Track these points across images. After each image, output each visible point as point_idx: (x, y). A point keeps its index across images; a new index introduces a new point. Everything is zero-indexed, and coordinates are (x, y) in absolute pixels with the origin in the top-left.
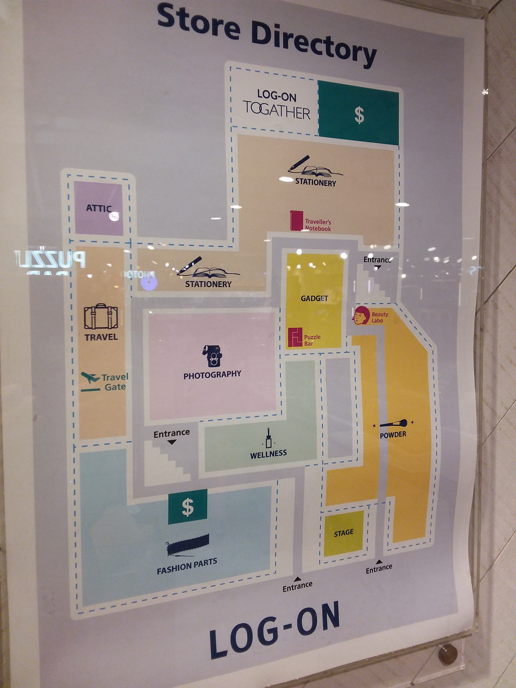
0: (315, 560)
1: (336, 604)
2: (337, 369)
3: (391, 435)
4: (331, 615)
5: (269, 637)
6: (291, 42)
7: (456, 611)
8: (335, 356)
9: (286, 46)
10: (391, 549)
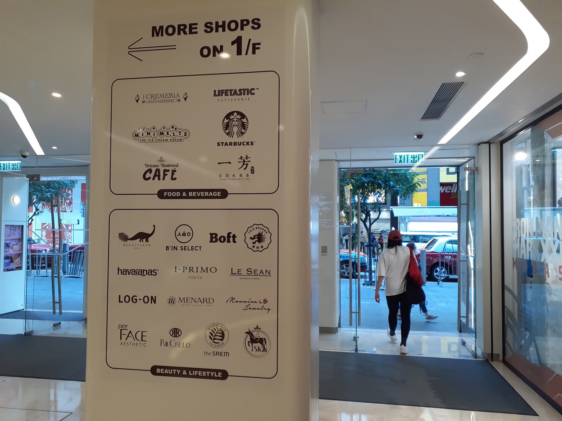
1: (227, 354)
5: (135, 301)
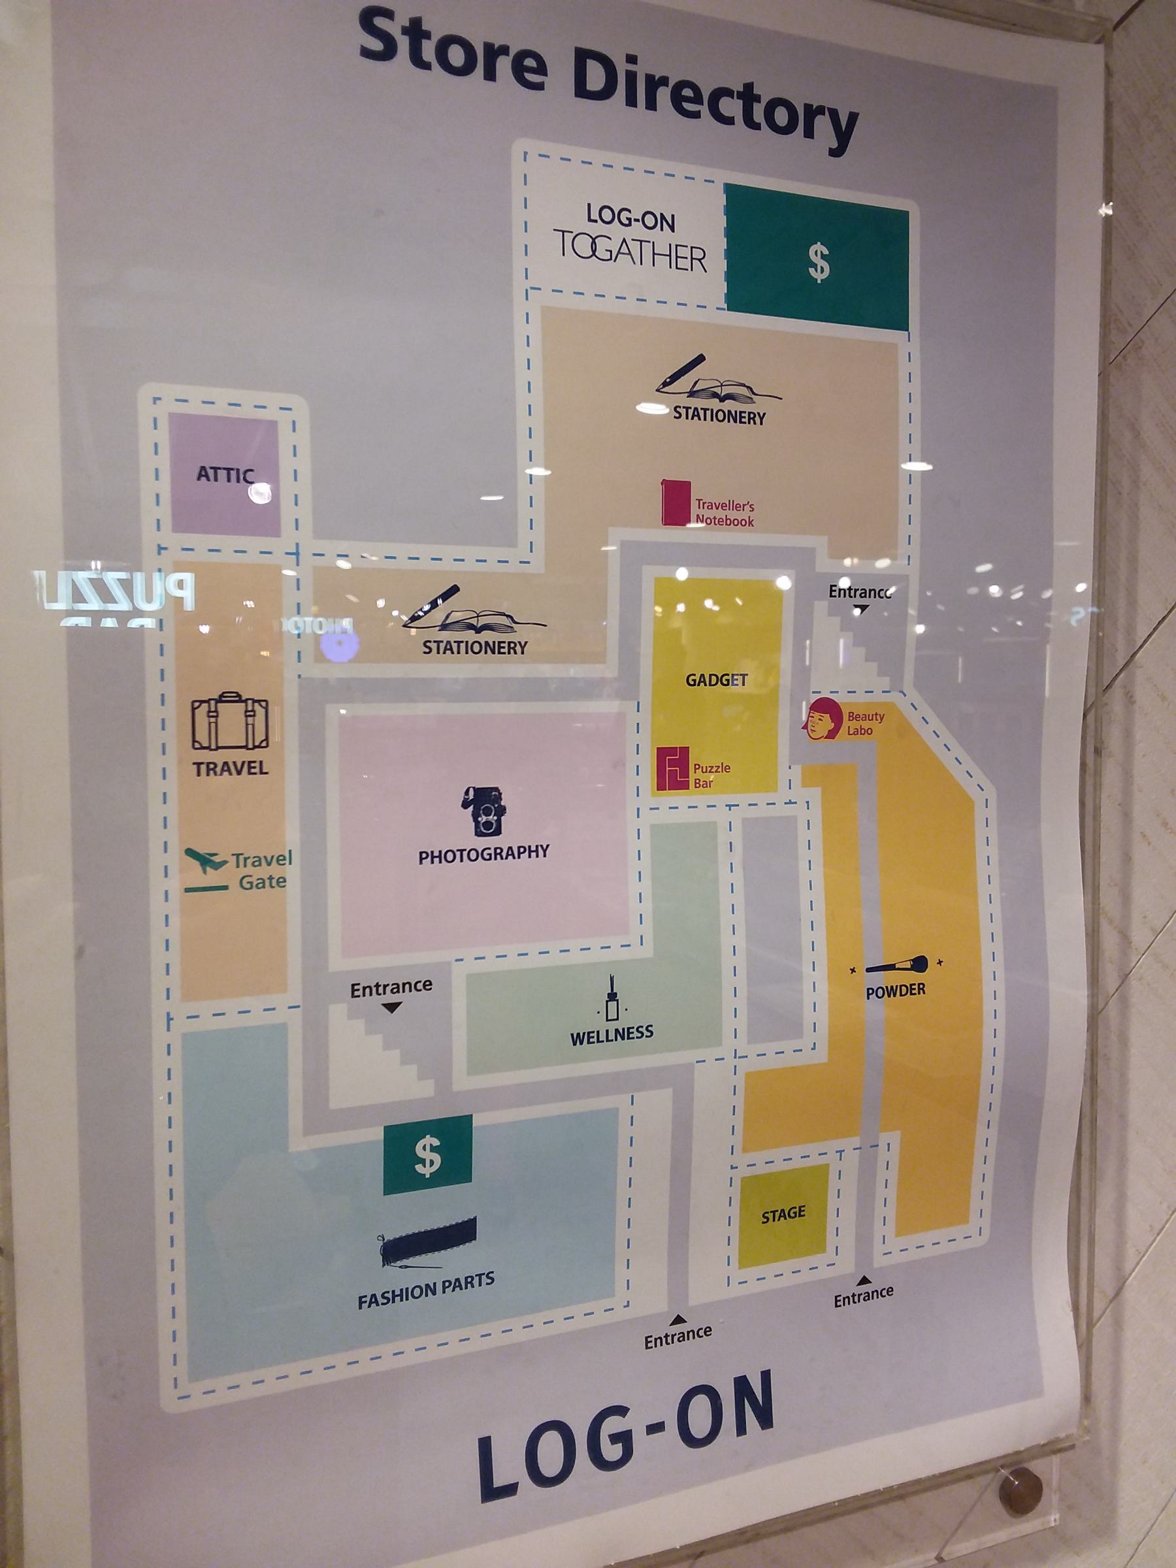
0: (717, 1276)
1: (766, 1376)
2: (769, 842)
3: (891, 991)
4: (755, 1402)
5: (612, 1452)
6: (664, 95)
7: (1039, 1393)
8: (763, 811)
9: (651, 105)
10: (892, 1252)
